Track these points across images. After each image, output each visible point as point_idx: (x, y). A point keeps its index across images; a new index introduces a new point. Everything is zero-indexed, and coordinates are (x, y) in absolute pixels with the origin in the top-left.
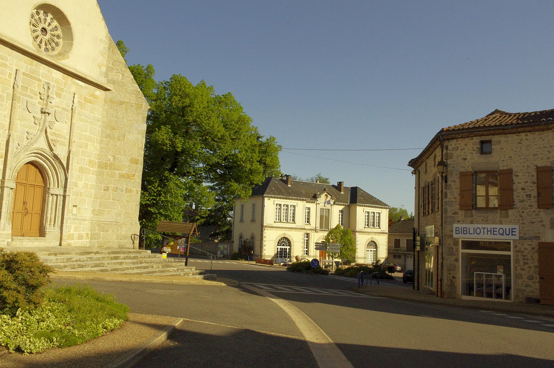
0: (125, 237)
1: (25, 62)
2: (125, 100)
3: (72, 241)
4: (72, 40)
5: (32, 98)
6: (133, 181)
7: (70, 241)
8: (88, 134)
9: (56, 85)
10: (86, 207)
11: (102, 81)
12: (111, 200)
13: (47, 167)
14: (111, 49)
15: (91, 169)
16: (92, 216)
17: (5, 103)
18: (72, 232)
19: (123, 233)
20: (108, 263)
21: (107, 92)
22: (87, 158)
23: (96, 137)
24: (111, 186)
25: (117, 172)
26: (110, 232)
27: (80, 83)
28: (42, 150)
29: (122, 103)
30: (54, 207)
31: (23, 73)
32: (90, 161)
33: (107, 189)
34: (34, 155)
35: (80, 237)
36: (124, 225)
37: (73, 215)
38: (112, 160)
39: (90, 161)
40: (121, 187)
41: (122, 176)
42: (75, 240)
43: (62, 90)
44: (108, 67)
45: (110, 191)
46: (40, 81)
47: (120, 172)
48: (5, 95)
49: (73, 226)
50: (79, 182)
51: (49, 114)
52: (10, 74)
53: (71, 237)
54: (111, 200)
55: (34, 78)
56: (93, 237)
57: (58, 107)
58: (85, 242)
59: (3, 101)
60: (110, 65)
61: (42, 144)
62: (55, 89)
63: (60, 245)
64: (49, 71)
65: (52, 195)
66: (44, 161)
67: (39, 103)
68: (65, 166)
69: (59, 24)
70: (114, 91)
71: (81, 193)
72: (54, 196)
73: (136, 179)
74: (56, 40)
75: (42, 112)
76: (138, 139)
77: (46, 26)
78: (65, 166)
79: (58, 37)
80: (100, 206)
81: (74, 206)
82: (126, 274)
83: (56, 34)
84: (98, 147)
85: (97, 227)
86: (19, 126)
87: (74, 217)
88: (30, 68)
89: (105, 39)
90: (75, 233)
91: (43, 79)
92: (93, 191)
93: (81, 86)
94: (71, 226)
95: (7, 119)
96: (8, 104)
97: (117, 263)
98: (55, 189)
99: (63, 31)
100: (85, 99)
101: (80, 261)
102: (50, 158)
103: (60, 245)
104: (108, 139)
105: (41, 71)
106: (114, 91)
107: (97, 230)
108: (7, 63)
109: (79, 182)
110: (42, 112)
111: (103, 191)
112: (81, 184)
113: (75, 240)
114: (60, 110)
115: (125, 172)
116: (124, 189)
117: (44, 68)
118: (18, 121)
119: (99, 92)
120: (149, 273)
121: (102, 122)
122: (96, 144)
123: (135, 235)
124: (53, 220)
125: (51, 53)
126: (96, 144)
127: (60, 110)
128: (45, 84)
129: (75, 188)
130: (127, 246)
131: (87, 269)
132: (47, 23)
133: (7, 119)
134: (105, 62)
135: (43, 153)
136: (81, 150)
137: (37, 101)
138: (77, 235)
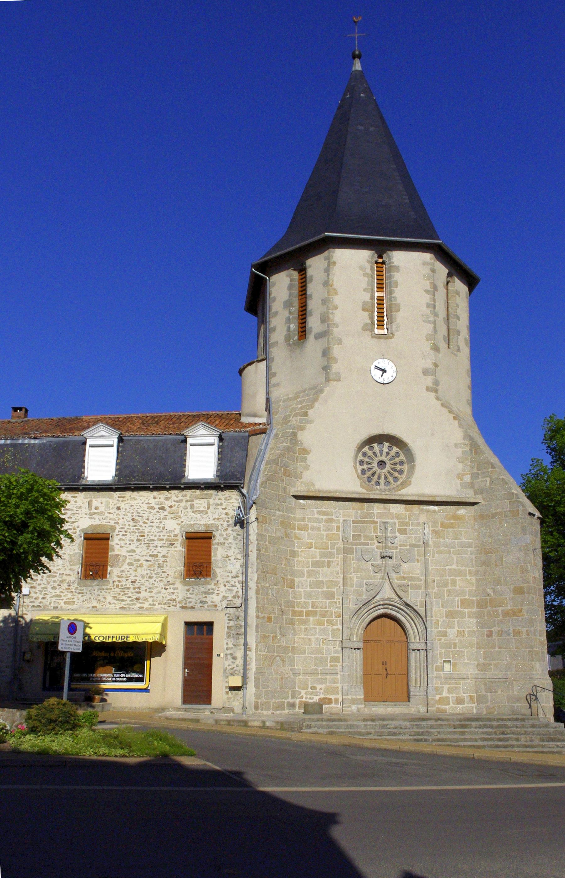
0: (518, 700)
1: (353, 509)
2: (498, 511)
3: (447, 707)
4: (413, 461)
5: (367, 544)
6: (520, 618)
7: (443, 707)
8: (454, 567)
9: (397, 521)
10: (466, 661)
11: (469, 496)
12: (497, 649)
14: (473, 450)
15: (466, 610)
16: (477, 672)
17: (335, 559)
19: (515, 693)
21: (476, 506)
22: (456, 599)
23: (467, 569)
24: (495, 629)
25: (500, 609)
26: (499, 692)
27: (432, 508)
28: (389, 599)
29: (494, 516)
30: (418, 665)
31: (353, 521)
32: (463, 602)
33: (490, 634)
34: (382, 607)
35: (460, 701)
36: (515, 682)
38: (492, 594)
39: (463, 602)
40: (506, 629)
41: (506, 614)
42: (452, 705)
43: (407, 524)
44: (472, 474)
45: (495, 637)
46: (376, 523)
47: (503, 608)
48: (335, 550)
49: (446, 687)
50: (449, 631)
51: (390, 558)
52: (338, 528)
54: (497, 649)
55: (367, 522)
56: (480, 700)
57: (404, 545)
58: (470, 708)
59: (334, 558)
60: (475, 471)
61: (387, 593)
62: (397, 525)
64: (385, 508)
65: (414, 650)
66: (398, 612)
67: (378, 548)
69: (398, 448)
70: (483, 502)
72: (416, 651)
73: (523, 615)
74: (398, 467)
75: (382, 558)
76: (519, 559)
77: (379, 458)
79: (401, 463)
80: (485, 658)
82: (459, 746)
83: (398, 462)
84: (474, 581)
85: (483, 687)
86: (355, 580)
88: (361, 513)
89: (462, 441)
90: (450, 696)
91: (379, 520)
92: (475, 639)
93: (434, 511)
94: (442, 688)
95: (340, 575)
96: (339, 560)
98: (415, 642)
99: (405, 455)
100: (442, 525)
101: (401, 728)
102: (401, 607)
104: (484, 567)
105: (375, 512)
106: (483, 502)
107: (483, 691)
108: (333, 517)
109: (449, 631)
110: (382, 558)
111: (485, 637)
113: (452, 705)
114: (408, 547)
115: (509, 608)
116: (511, 631)
117: (377, 508)
119: (462, 511)
120: (505, 747)
121: (475, 547)
122: (468, 578)
123: (530, 694)
124: (419, 681)
125: (393, 485)
126: (468, 578)
127: (408, 547)
128: (382, 524)
129: (443, 638)
130: (523, 711)
131: (405, 737)
132: (384, 454)
133: (340, 575)
134: (468, 469)
135: (392, 603)
136: (446, 589)
137: (375, 546)
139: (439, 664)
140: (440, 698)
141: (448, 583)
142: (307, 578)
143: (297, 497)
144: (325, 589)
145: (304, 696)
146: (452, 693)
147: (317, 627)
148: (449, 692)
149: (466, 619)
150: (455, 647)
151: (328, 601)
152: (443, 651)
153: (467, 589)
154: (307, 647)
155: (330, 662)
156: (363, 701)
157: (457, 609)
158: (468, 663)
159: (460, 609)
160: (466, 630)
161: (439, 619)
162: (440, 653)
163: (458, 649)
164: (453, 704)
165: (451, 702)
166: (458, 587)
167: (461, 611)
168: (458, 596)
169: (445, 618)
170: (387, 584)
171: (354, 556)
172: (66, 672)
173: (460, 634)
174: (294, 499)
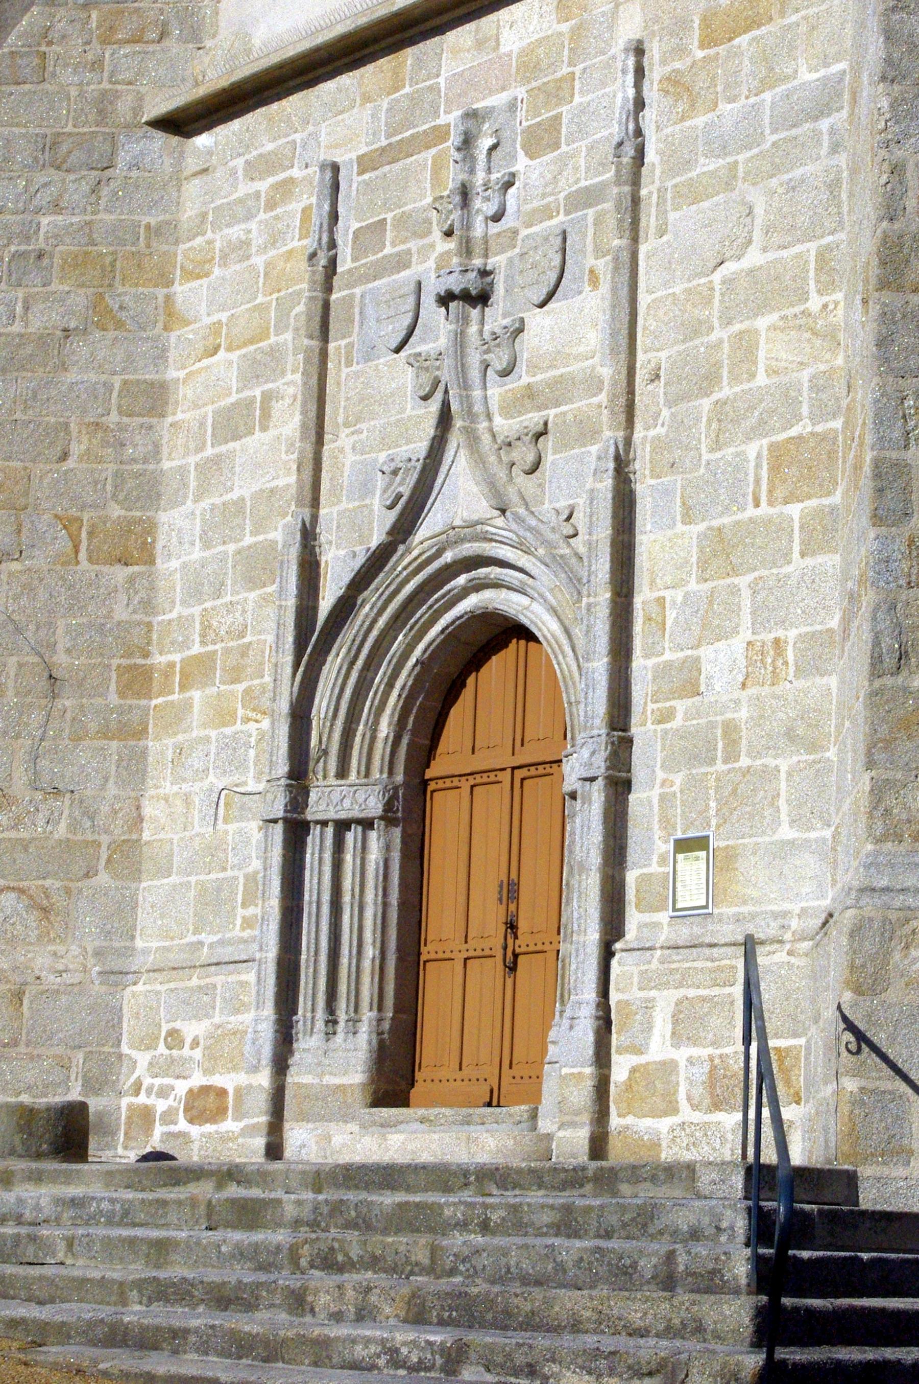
3: (664, 1125)
10: (786, 832)
13: (421, 646)
15: (795, 510)
18: (659, 1048)
20: (70, 1243)
22: (752, 450)
37: (681, 915)
42: (687, 1113)
53: (657, 1086)
63: (274, 1151)
68: (325, 605)
71: (730, 729)
78: (325, 605)
81: (684, 846)
87: (684, 933)
90: (682, 1055)
94: (648, 1006)
97: (132, 1242)
103: (274, 1151)
112: (721, 662)
113: (687, 1113)
118: (621, 342)
129: (681, 706)
138: (701, 1073)
139: (655, 868)
140: (633, 1070)
141: (718, 365)
142: (195, 502)
143: (181, 123)
144: (248, 540)
145: (147, 1081)
146: (694, 1041)
147: (213, 734)
148: (677, 1038)
149: (797, 564)
150: (731, 756)
151: (253, 595)
152: (678, 779)
153: (805, 375)
154: (176, 838)
155: (244, 905)
156: (358, 1098)
157: (751, 512)
158: (792, 842)
159: (764, 509)
160: (792, 634)
161: (668, 594)
162: (663, 798)
163: (744, 761)
164: (695, 1107)
165: (682, 1095)
166: (761, 379)
167: (768, 521)
168: (760, 429)
169: (693, 586)
170: (463, 459)
171: (354, 338)
172: (395, 921)
173: (764, 660)
174: (160, 138)
